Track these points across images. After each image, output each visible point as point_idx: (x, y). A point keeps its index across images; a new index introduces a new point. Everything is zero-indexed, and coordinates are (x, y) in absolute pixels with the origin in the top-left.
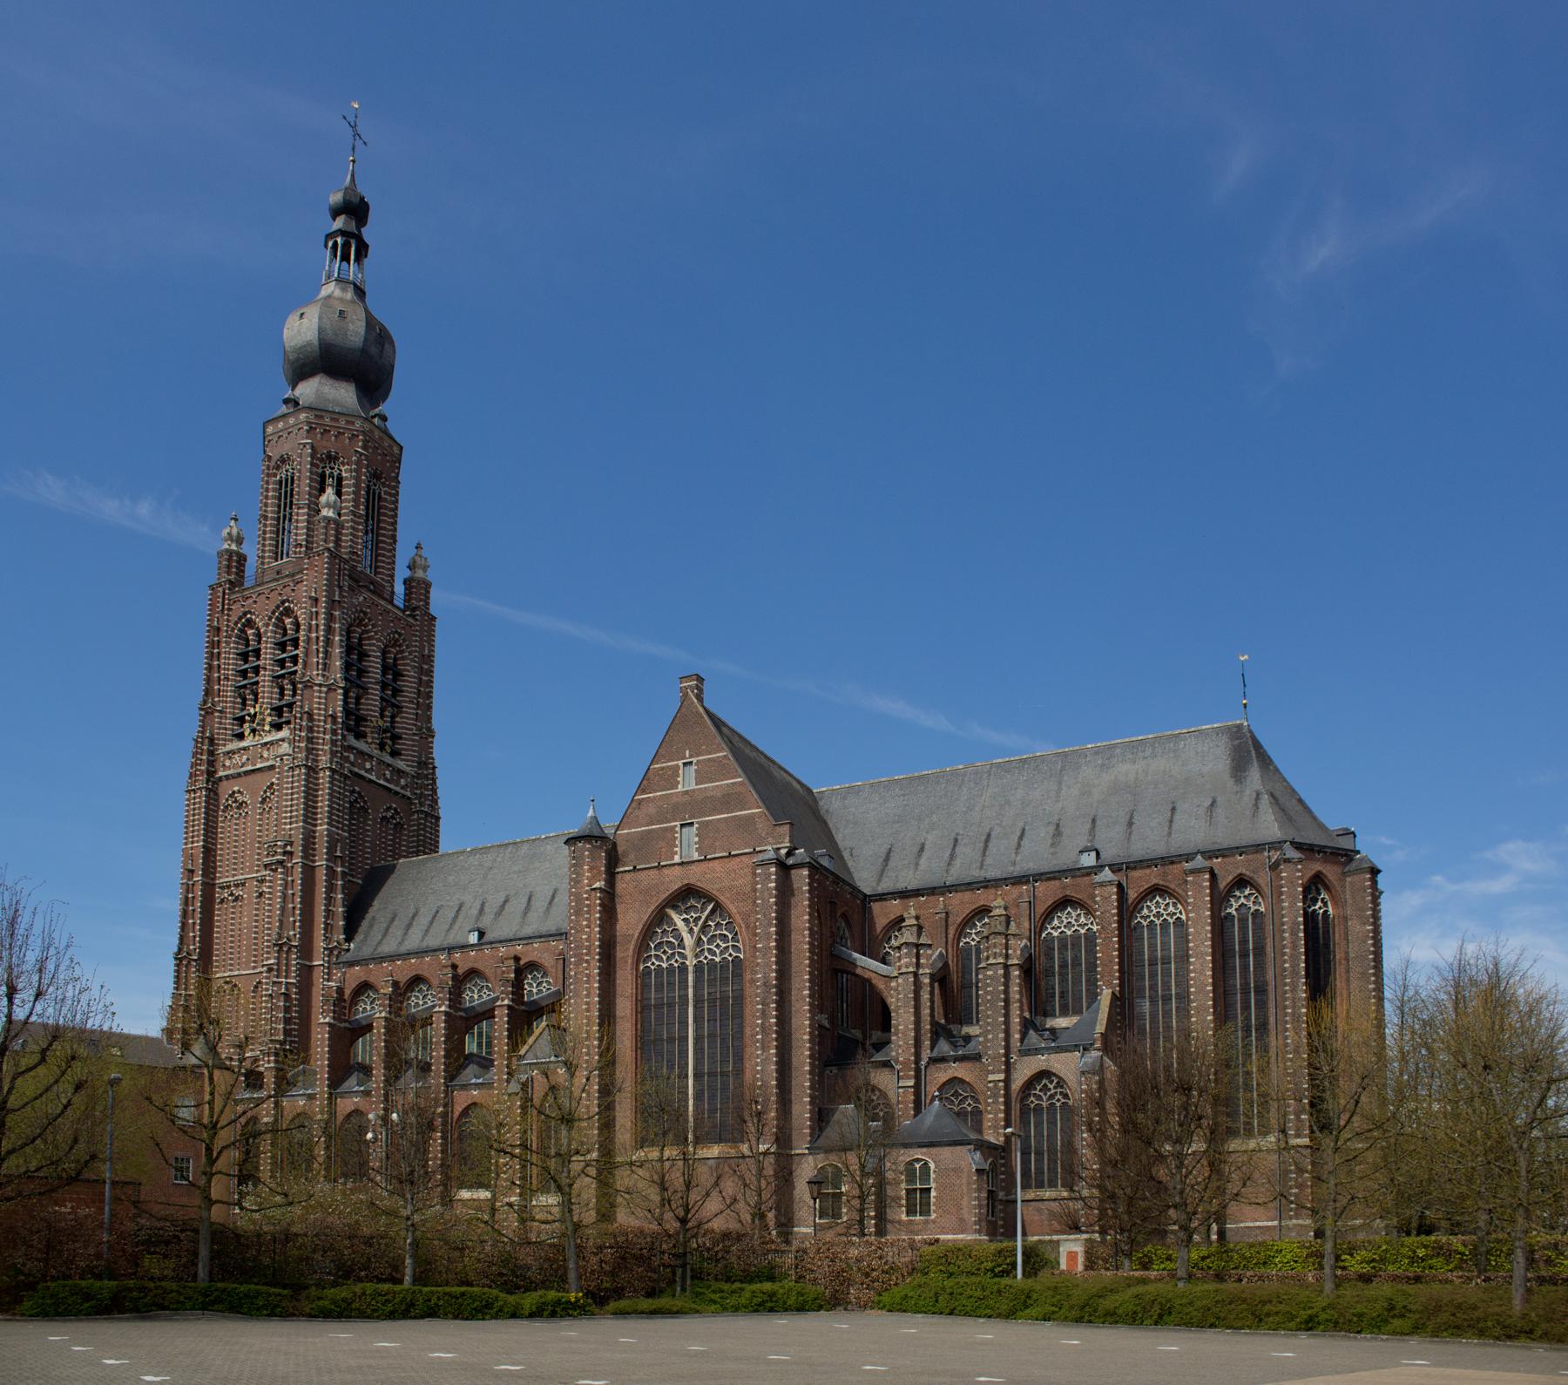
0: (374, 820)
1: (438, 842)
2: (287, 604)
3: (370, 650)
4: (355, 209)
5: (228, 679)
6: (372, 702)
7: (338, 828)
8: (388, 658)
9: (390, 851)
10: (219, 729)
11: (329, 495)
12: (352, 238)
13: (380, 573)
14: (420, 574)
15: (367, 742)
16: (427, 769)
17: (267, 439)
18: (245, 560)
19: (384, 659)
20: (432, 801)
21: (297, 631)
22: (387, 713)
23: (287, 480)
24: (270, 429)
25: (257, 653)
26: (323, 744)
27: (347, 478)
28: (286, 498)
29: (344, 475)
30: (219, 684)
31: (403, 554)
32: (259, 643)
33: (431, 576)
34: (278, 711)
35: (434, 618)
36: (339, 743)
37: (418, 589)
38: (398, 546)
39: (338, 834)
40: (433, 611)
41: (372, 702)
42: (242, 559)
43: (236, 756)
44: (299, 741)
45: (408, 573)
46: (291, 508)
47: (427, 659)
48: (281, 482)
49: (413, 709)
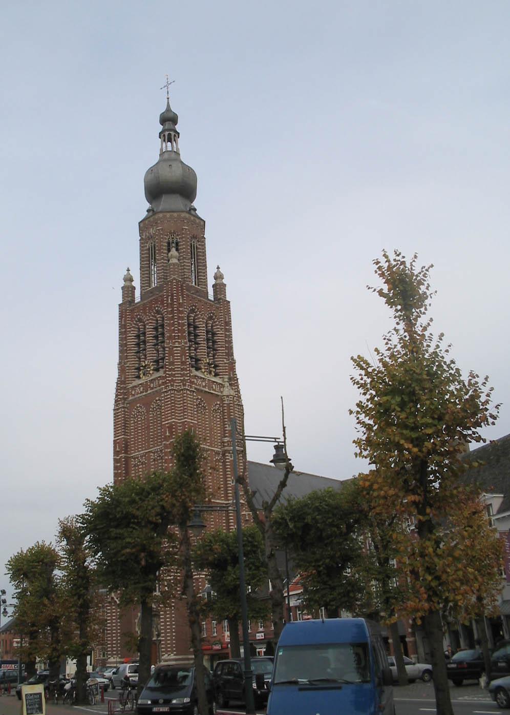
7: (192, 419)
18: (135, 289)
19: (207, 327)
22: (210, 355)
25: (144, 334)
26: (178, 339)
29: (178, 240)
31: (211, 273)
33: (224, 281)
34: (157, 362)
35: (229, 302)
37: (220, 288)
39: (192, 423)
44: (168, 377)
47: (228, 323)
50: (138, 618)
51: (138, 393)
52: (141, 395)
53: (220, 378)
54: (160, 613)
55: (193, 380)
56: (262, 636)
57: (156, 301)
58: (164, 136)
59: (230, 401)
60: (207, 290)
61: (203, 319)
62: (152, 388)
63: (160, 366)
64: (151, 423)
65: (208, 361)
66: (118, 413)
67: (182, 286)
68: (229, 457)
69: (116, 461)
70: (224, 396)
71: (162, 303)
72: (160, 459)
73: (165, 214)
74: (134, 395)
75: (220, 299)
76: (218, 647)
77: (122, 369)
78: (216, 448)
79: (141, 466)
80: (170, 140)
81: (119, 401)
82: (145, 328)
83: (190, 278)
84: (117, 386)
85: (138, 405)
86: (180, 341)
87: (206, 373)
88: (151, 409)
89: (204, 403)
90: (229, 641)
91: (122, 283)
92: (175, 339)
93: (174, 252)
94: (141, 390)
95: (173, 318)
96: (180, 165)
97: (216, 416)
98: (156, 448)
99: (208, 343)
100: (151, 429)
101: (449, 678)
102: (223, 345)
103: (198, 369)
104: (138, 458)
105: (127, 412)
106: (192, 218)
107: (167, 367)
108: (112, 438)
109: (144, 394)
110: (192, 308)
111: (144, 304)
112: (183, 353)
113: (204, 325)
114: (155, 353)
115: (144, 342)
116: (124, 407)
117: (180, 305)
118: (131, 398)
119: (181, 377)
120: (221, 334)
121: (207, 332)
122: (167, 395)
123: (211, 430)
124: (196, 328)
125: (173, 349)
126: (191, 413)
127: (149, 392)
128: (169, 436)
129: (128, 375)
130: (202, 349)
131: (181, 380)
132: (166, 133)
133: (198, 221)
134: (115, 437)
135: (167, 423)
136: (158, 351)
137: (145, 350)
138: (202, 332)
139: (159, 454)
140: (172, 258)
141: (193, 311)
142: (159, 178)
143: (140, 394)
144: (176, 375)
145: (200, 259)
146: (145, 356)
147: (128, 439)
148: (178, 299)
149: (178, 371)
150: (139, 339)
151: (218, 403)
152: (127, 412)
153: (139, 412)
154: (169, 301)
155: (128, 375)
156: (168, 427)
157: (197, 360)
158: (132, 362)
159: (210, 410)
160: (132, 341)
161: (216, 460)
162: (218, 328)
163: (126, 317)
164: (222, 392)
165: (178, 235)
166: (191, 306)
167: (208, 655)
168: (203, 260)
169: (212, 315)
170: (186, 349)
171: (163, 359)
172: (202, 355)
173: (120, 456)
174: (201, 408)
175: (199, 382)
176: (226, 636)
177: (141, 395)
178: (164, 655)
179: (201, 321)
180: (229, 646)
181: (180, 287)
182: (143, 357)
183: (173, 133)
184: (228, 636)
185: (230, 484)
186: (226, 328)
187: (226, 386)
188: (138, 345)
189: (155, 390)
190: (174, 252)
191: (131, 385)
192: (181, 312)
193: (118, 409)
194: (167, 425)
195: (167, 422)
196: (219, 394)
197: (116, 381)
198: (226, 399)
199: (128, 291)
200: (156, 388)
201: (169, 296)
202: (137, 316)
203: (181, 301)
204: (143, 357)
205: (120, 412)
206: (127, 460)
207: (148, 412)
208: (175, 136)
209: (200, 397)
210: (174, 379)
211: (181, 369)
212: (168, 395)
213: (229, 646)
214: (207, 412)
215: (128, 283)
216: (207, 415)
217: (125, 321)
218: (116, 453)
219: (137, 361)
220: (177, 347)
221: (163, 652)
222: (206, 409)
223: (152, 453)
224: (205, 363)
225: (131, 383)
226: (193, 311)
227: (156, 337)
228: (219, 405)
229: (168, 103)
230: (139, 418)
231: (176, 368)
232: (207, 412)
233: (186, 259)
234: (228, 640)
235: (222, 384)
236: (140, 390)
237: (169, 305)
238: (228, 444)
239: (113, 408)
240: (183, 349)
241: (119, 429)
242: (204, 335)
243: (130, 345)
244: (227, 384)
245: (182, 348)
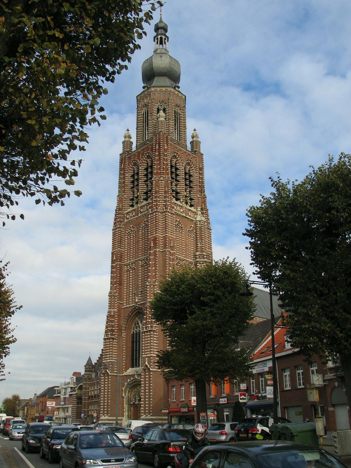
1: (211, 248)
3: (180, 167)
4: (228, 257)
7: (171, 235)
8: (187, 170)
13: (181, 140)
14: (195, 139)
15: (181, 202)
18: (132, 144)
19: (185, 170)
20: (208, 223)
22: (187, 191)
25: (138, 174)
26: (163, 175)
28: (145, 123)
29: (165, 107)
31: (189, 132)
34: (146, 193)
35: (202, 155)
37: (195, 144)
38: (187, 130)
39: (171, 237)
40: (202, 152)
45: (191, 140)
48: (144, 114)
50: (125, 386)
51: (131, 217)
53: (194, 208)
54: (141, 382)
55: (173, 206)
56: (225, 401)
57: (147, 149)
58: (157, 39)
59: (202, 225)
60: (186, 144)
61: (182, 163)
62: (142, 212)
65: (185, 194)
66: (116, 232)
67: (167, 137)
69: (112, 267)
70: (197, 221)
71: (152, 150)
73: (156, 88)
75: (195, 151)
76: (185, 410)
77: (120, 200)
78: (190, 259)
80: (161, 43)
81: (117, 223)
82: (138, 170)
83: (173, 134)
84: (116, 212)
85: (131, 226)
86: (164, 176)
87: (183, 203)
89: (182, 225)
90: (196, 405)
91: (123, 139)
92: (160, 175)
93: (162, 113)
95: (160, 164)
96: (168, 56)
97: (191, 235)
98: (143, 257)
99: (185, 176)
102: (198, 184)
103: (177, 199)
105: (123, 231)
106: (176, 92)
108: (110, 251)
110: (175, 155)
111: (139, 153)
112: (166, 185)
113: (183, 168)
114: (145, 187)
115: (138, 180)
116: (120, 227)
117: (165, 150)
118: (126, 221)
120: (196, 176)
121: (186, 173)
122: (152, 216)
123: (186, 245)
124: (177, 169)
126: (171, 230)
127: (139, 215)
128: (153, 246)
129: (125, 204)
130: (181, 185)
132: (159, 37)
133: (180, 95)
134: (112, 250)
136: (147, 186)
138: (181, 173)
140: (160, 117)
141: (175, 157)
143: (133, 217)
145: (181, 122)
146: (138, 190)
147: (123, 251)
148: (164, 146)
149: (162, 198)
150: (134, 178)
151: (193, 226)
152: (123, 231)
153: (132, 231)
154: (157, 148)
156: (153, 240)
157: (177, 193)
158: (129, 195)
160: (129, 179)
162: (194, 172)
163: (125, 163)
164: (195, 218)
165: (165, 104)
166: (173, 153)
167: (177, 416)
168: (184, 122)
169: (189, 161)
170: (169, 182)
171: (150, 191)
172: (181, 189)
174: (179, 228)
175: (178, 208)
176: (192, 401)
178: (143, 415)
179: (181, 165)
180: (195, 409)
181: (165, 138)
182: (136, 191)
183: (164, 37)
184: (194, 401)
186: (200, 173)
187: (199, 214)
188: (133, 182)
189: (144, 213)
190: (162, 113)
191: (126, 212)
192: (166, 156)
193: (116, 229)
195: (152, 236)
196: (194, 219)
197: (107, 315)
198: (198, 223)
199: (127, 144)
202: (133, 161)
203: (166, 148)
204: (136, 191)
205: (117, 231)
208: (165, 39)
209: (178, 220)
210: (159, 204)
211: (164, 196)
212: (154, 216)
213: (195, 409)
214: (184, 232)
215: (127, 139)
216: (183, 234)
217: (124, 165)
218: (113, 261)
219: (131, 194)
221: (142, 413)
222: (183, 230)
223: (140, 261)
224: (183, 196)
225: (127, 210)
226: (175, 157)
227: (146, 175)
228: (193, 227)
229: (161, 17)
231: (160, 196)
232: (184, 232)
233: (171, 120)
234: (194, 404)
235: (196, 213)
237: (157, 151)
238: (199, 257)
239: (103, 338)
240: (166, 182)
241: (107, 358)
242: (183, 175)
243: (127, 178)
244: (199, 213)
245: (165, 181)
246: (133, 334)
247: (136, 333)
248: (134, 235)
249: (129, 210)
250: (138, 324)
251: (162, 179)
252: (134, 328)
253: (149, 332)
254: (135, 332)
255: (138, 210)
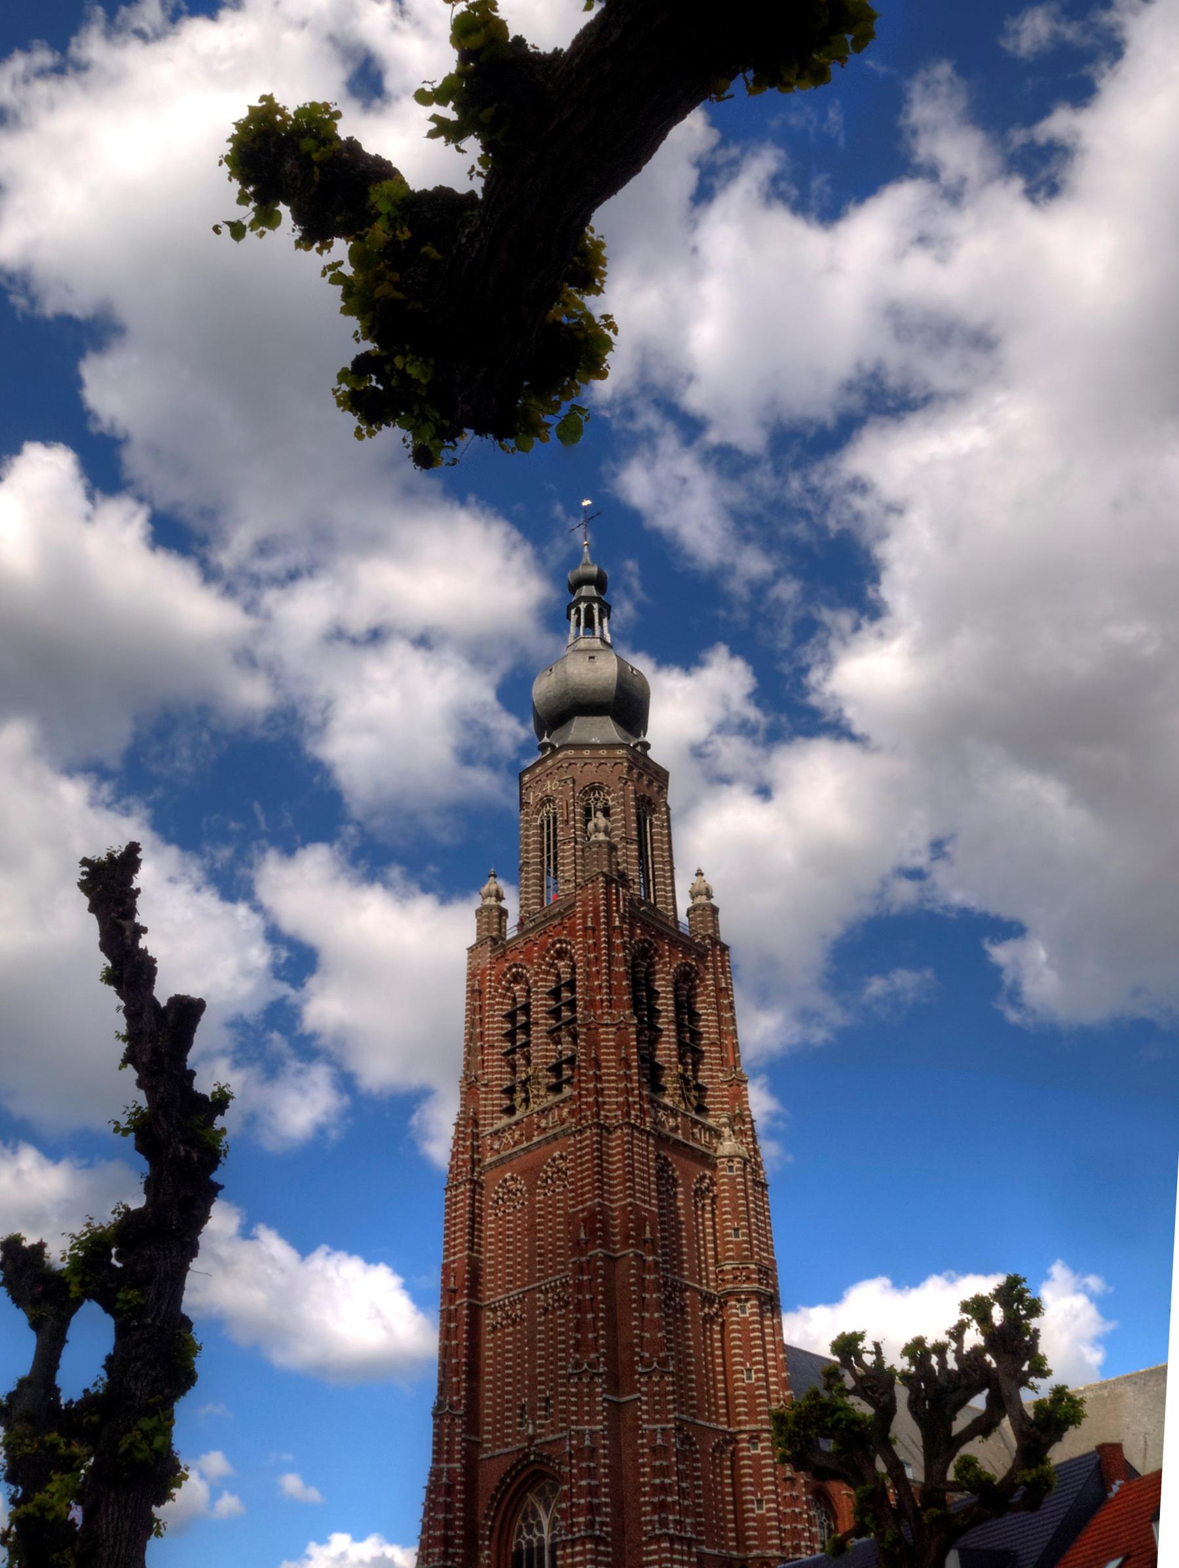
0: (685, 1193)
2: (558, 946)
5: (493, 1047)
6: (666, 1052)
9: (561, 1325)
10: (486, 1099)
11: (600, 820)
12: (595, 602)
16: (744, 1123)
17: (524, 787)
21: (574, 972)
23: (548, 822)
24: (526, 778)
27: (614, 807)
29: (610, 803)
30: (482, 1054)
32: (528, 996)
36: (636, 1092)
40: (724, 937)
41: (666, 1052)
42: (503, 913)
43: (506, 1134)
44: (586, 1096)
46: (555, 847)
48: (542, 826)
49: (716, 1052)
52: (516, 1149)
63: (565, 1077)
64: (540, 1216)
68: (739, 1312)
72: (560, 1308)
74: (498, 1151)
79: (511, 1329)
84: (457, 1132)
86: (615, 1012)
88: (539, 1183)
94: (516, 1136)
100: (540, 1231)
101: (1009, 1278)
104: (502, 1308)
107: (583, 1071)
109: (525, 1145)
115: (526, 1028)
119: (617, 1096)
125: (596, 1029)
131: (617, 1089)
135: (582, 1210)
137: (527, 1044)
139: (558, 1294)
142: (567, 680)
143: (513, 1146)
144: (606, 1092)
155: (485, 1106)
156: (584, 1220)
158: (496, 1074)
159: (688, 1187)
161: (706, 1315)
165: (609, 793)
173: (458, 1302)
177: (516, 1149)
185: (743, 1380)
188: (511, 1036)
191: (490, 1130)
194: (581, 1215)
200: (552, 1128)
201: (589, 912)
206: (475, 1312)
207: (531, 1192)
212: (586, 1139)
220: (607, 1025)
223: (541, 1292)
230: (509, 1207)
236: (513, 1138)
246: (519, 1551)
247: (530, 1550)
248: (518, 1207)
249: (499, 1125)
250: (535, 1515)
251: (607, 1020)
252: (520, 1532)
253: (579, 1542)
254: (524, 1547)
255: (531, 1123)
